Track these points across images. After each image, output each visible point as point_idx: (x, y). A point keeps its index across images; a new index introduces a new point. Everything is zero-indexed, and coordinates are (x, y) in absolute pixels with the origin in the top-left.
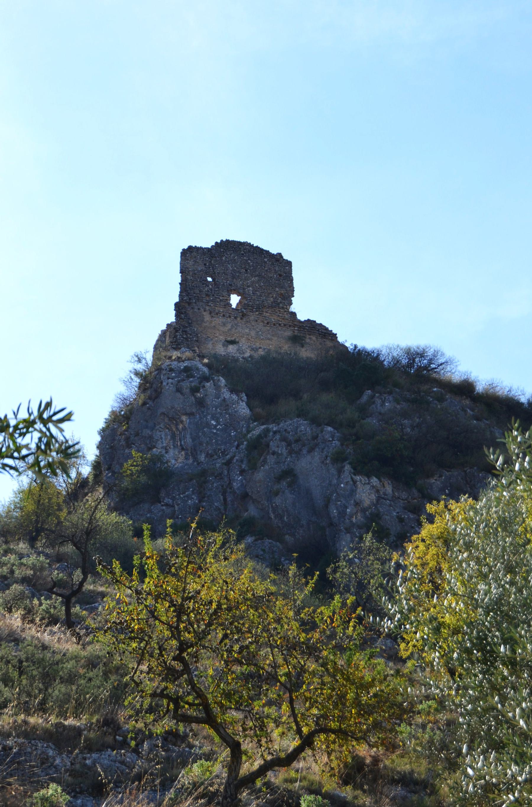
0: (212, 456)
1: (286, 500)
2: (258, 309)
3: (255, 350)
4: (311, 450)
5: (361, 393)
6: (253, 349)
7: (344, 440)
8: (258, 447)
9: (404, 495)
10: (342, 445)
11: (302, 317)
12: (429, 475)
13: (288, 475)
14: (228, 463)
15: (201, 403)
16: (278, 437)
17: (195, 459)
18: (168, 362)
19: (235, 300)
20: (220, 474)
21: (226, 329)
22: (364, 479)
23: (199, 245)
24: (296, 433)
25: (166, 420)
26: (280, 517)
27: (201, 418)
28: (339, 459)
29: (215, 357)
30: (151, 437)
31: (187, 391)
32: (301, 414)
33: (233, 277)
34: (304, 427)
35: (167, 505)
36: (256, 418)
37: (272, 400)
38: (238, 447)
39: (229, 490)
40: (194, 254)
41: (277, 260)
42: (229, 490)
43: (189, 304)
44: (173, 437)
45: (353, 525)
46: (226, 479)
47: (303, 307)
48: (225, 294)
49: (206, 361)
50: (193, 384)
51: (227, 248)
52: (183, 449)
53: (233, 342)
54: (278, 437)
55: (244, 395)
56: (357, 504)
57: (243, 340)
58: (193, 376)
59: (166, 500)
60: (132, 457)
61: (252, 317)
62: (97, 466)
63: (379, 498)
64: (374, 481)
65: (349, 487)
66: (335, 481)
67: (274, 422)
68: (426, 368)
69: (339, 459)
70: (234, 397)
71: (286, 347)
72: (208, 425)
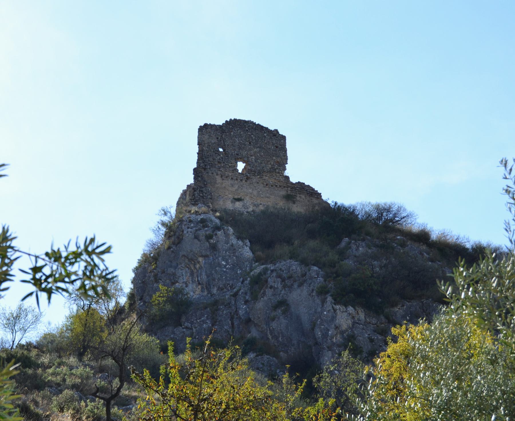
0: (222, 289)
1: (281, 324)
2: (259, 173)
3: (257, 206)
4: (300, 285)
5: (340, 240)
6: (255, 205)
7: (326, 277)
8: (259, 282)
9: (374, 321)
10: (325, 281)
11: (294, 180)
12: (394, 305)
13: (282, 304)
14: (235, 295)
15: (214, 247)
16: (274, 274)
17: (209, 292)
18: (188, 215)
19: (241, 166)
20: (229, 304)
21: (234, 189)
22: (343, 308)
23: (212, 123)
24: (289, 272)
25: (187, 261)
26: (276, 337)
27: (214, 259)
28: (323, 292)
29: (225, 211)
30: (174, 274)
31: (202, 238)
32: (293, 256)
33: (240, 148)
34: (295, 267)
35: (187, 328)
36: (257, 259)
37: (269, 245)
38: (243, 282)
39: (235, 316)
40: (209, 130)
41: (275, 135)
42: (235, 316)
43: (205, 169)
44: (192, 274)
45: (334, 344)
46: (233, 308)
47: (295, 172)
48: (233, 161)
49: (218, 214)
50: (208, 233)
51: (234, 124)
52: (199, 284)
53: (239, 200)
54: (274, 274)
55: (248, 241)
56: (337, 328)
57: (247, 198)
58: (207, 226)
59: (186, 324)
60: (159, 290)
61: (255, 179)
62: (131, 297)
63: (354, 323)
64: (351, 309)
65: (330, 314)
66: (319, 310)
67: (271, 262)
68: (391, 220)
69: (323, 292)
70: (240, 243)
71: (281, 204)
72: (219, 265)
